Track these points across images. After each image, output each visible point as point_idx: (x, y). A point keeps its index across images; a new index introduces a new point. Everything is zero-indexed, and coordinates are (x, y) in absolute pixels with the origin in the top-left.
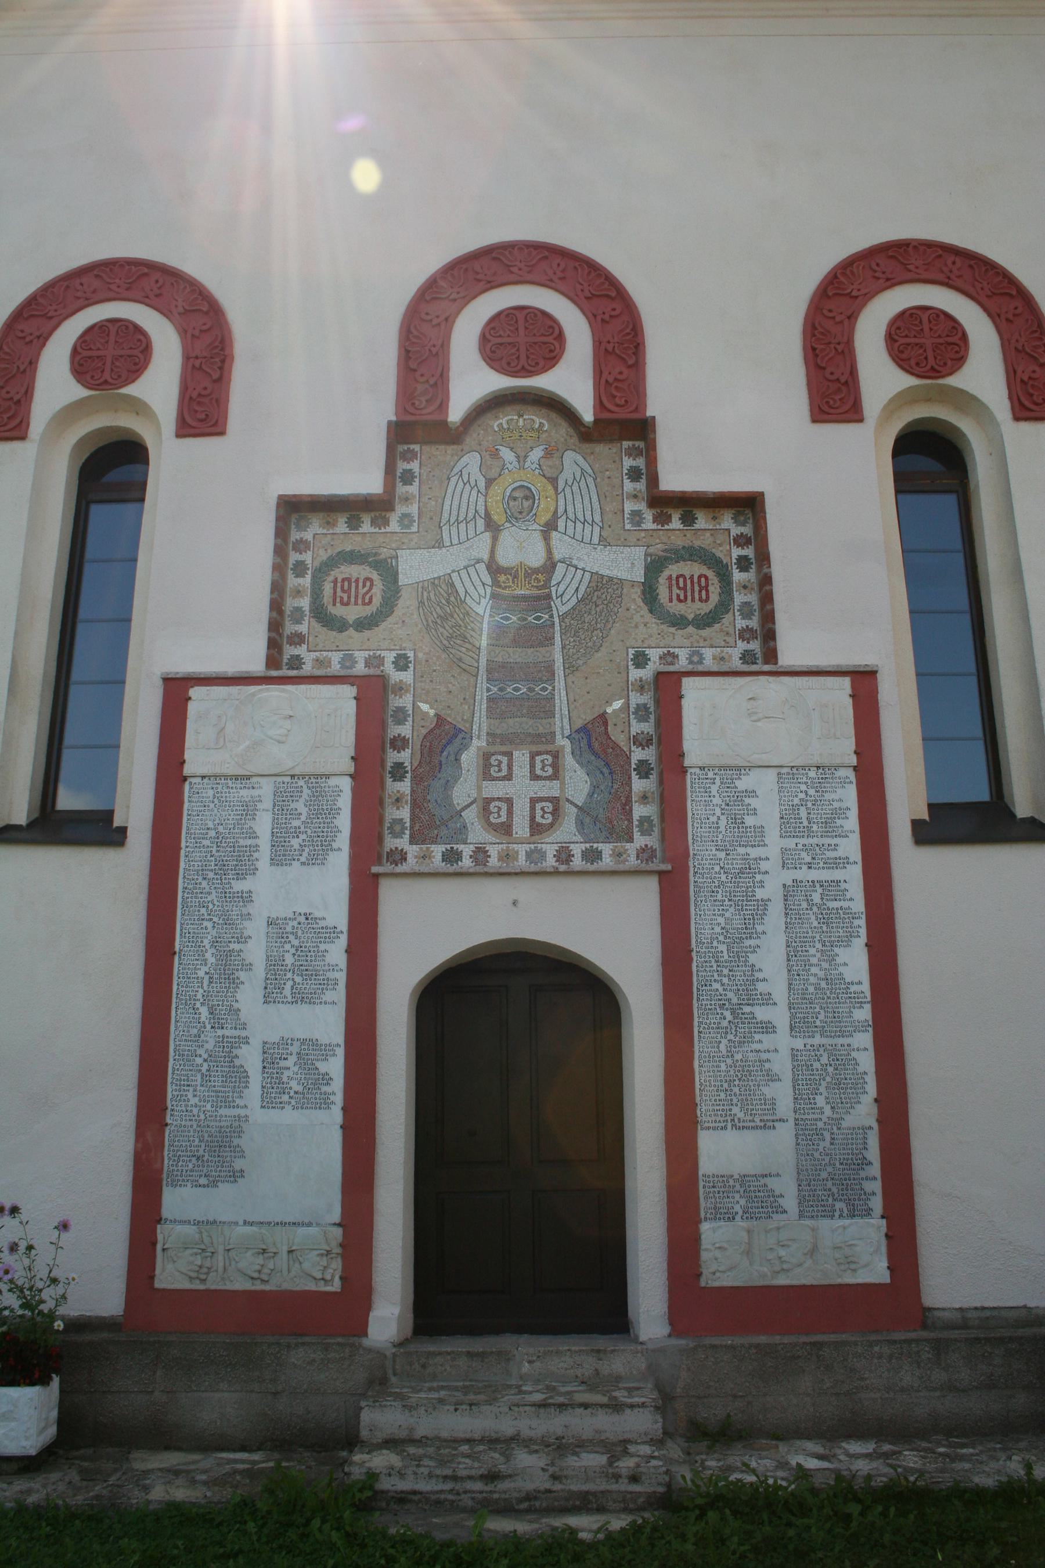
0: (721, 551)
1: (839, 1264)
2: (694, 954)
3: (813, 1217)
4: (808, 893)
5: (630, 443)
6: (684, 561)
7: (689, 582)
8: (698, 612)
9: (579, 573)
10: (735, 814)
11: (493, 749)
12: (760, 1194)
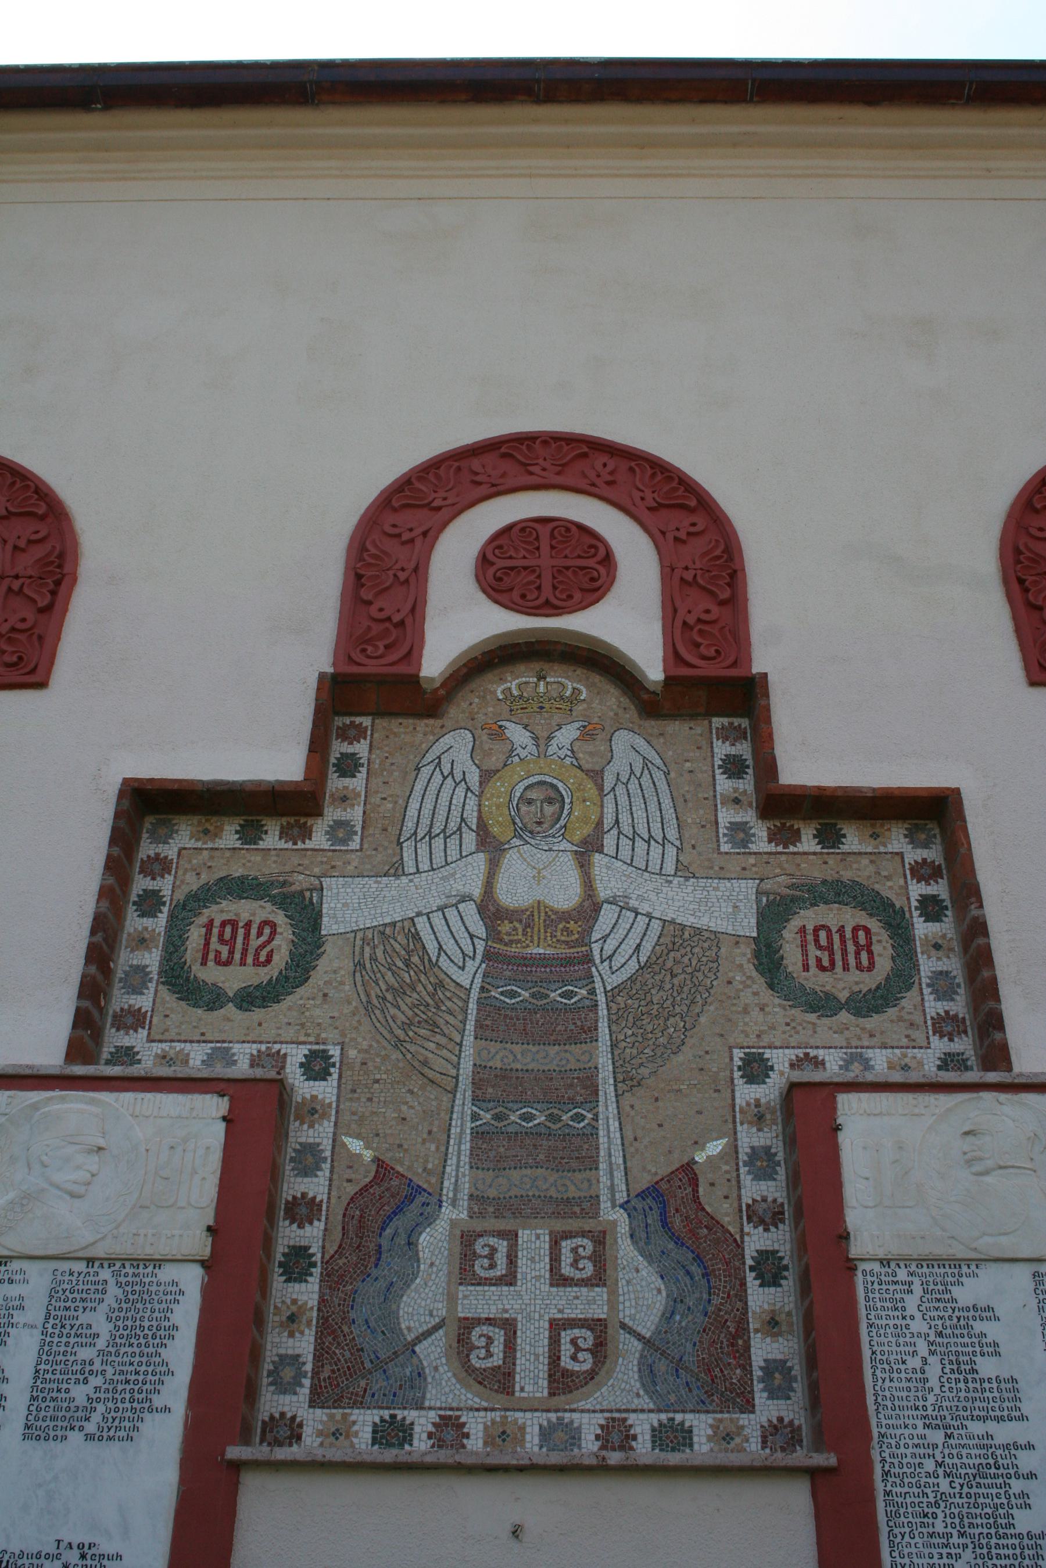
0: (891, 888)
5: (725, 721)
6: (825, 903)
7: (836, 938)
8: (856, 989)
9: (642, 921)
11: (478, 1226)
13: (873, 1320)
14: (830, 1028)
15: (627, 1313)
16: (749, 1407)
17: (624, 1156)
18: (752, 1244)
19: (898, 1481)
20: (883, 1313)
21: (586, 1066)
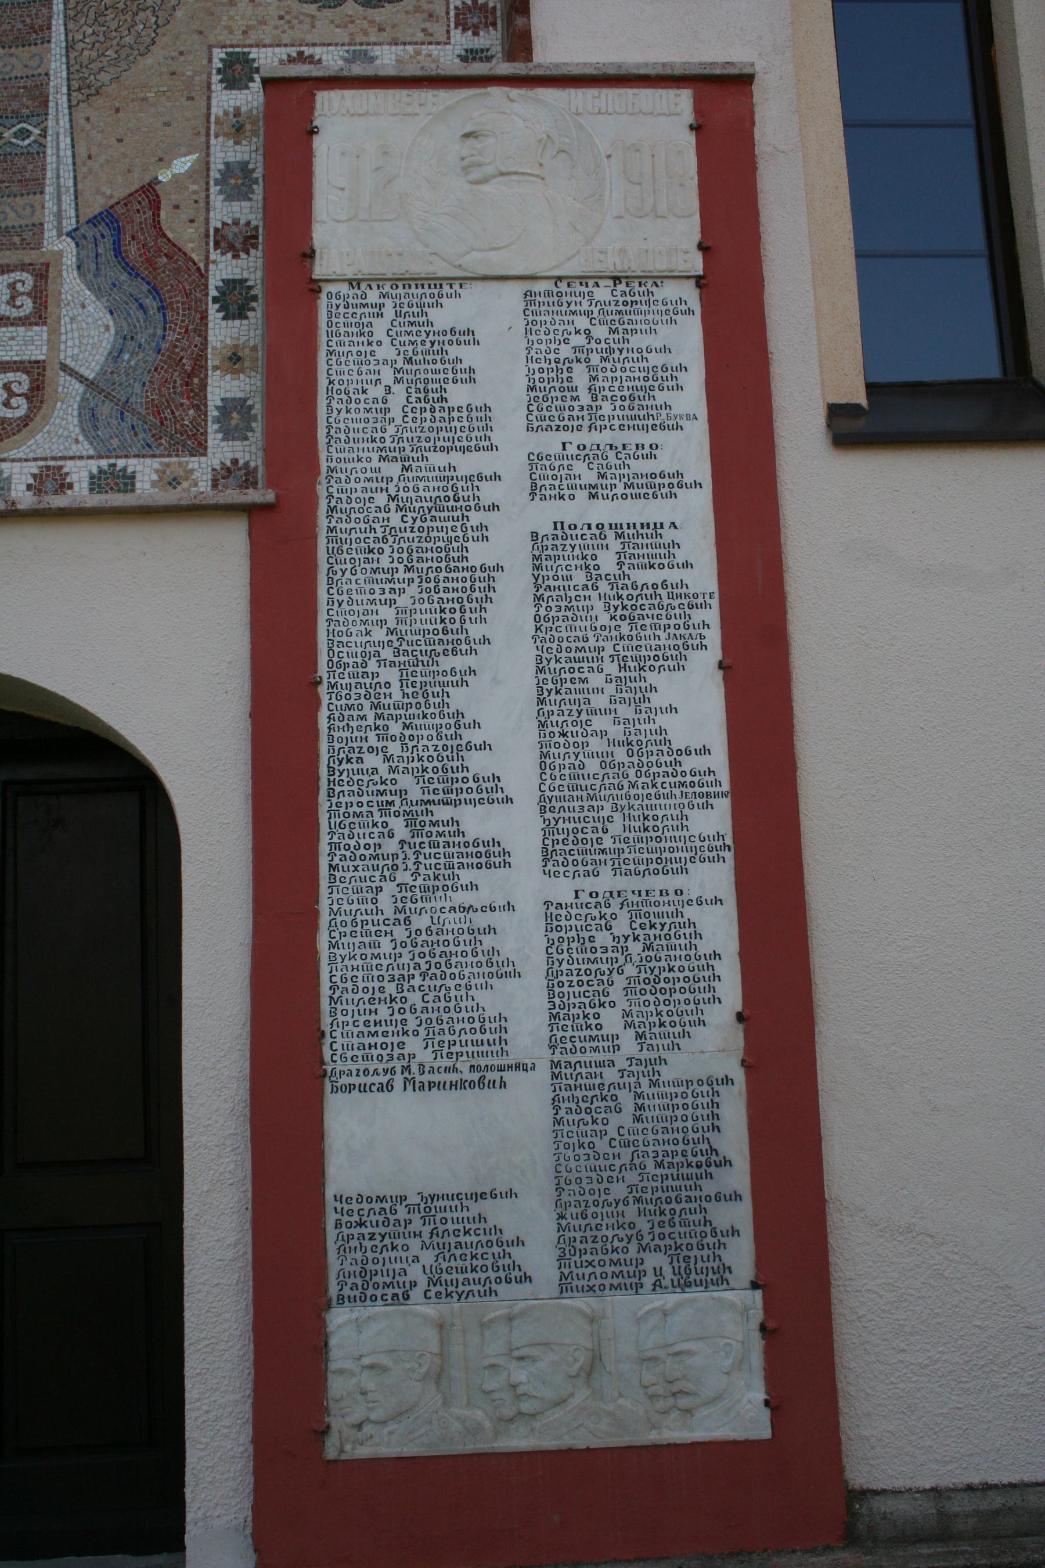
1: (652, 1397)
2: (323, 690)
3: (591, 1288)
4: (590, 552)
10: (426, 381)
12: (468, 1239)
13: (335, 347)
14: (332, 22)
15: (69, 352)
16: (200, 448)
17: (75, 177)
18: (218, 273)
19: (344, 517)
20: (347, 339)
21: (36, 73)
